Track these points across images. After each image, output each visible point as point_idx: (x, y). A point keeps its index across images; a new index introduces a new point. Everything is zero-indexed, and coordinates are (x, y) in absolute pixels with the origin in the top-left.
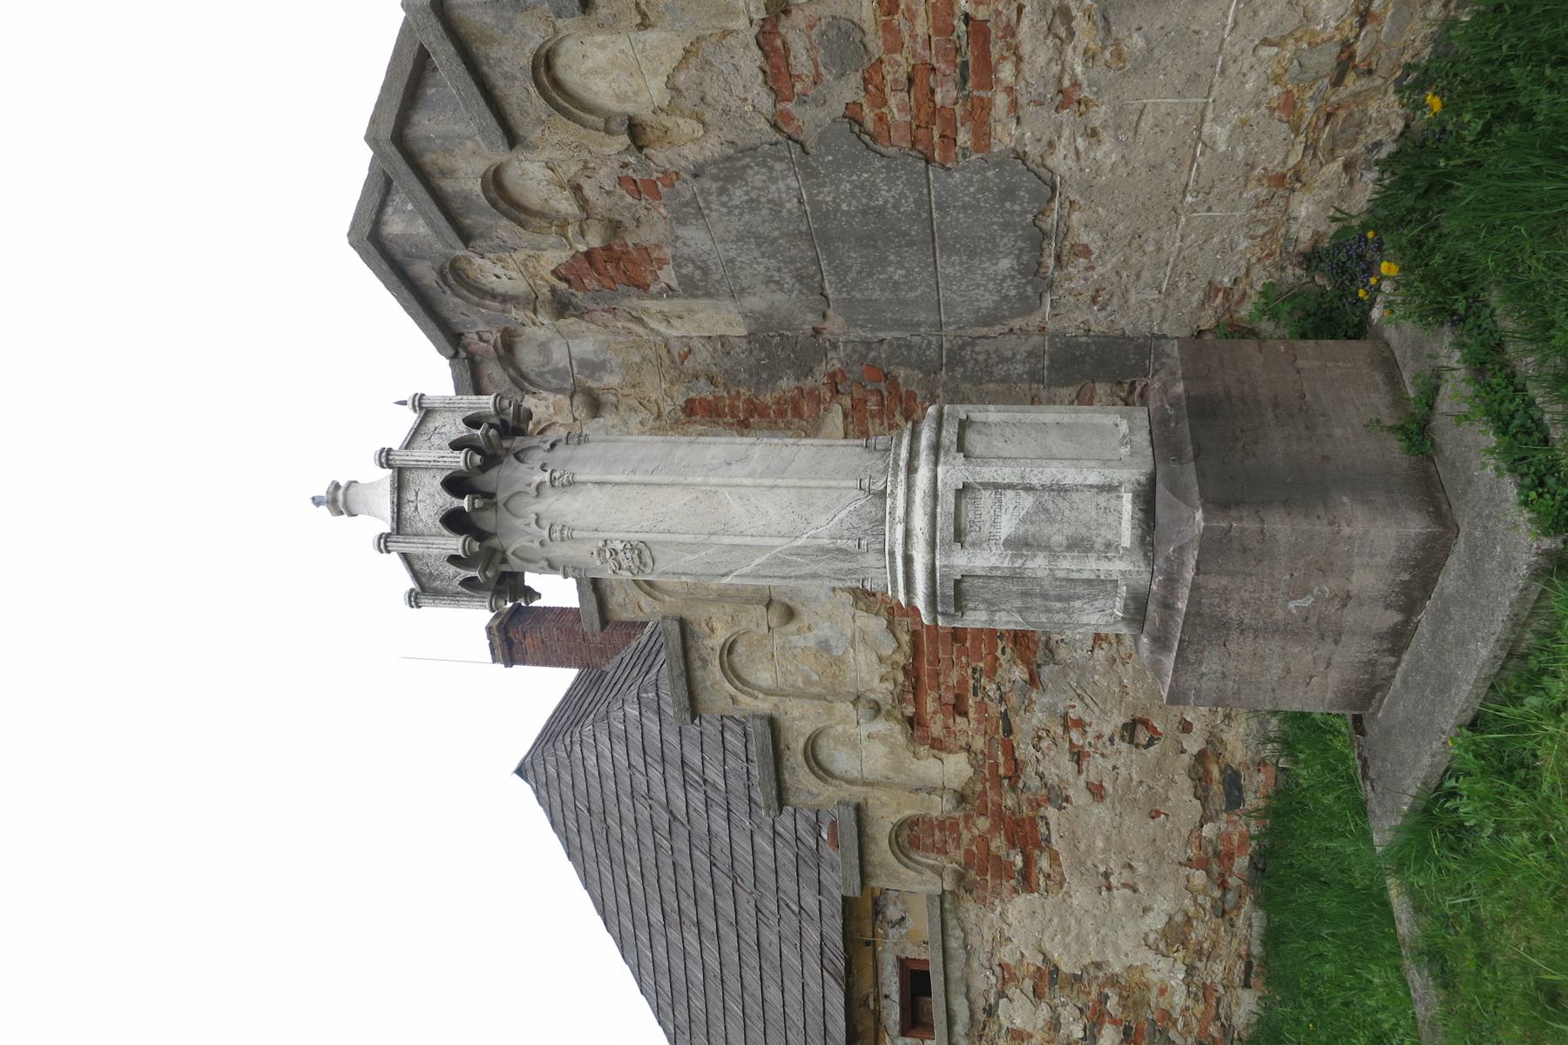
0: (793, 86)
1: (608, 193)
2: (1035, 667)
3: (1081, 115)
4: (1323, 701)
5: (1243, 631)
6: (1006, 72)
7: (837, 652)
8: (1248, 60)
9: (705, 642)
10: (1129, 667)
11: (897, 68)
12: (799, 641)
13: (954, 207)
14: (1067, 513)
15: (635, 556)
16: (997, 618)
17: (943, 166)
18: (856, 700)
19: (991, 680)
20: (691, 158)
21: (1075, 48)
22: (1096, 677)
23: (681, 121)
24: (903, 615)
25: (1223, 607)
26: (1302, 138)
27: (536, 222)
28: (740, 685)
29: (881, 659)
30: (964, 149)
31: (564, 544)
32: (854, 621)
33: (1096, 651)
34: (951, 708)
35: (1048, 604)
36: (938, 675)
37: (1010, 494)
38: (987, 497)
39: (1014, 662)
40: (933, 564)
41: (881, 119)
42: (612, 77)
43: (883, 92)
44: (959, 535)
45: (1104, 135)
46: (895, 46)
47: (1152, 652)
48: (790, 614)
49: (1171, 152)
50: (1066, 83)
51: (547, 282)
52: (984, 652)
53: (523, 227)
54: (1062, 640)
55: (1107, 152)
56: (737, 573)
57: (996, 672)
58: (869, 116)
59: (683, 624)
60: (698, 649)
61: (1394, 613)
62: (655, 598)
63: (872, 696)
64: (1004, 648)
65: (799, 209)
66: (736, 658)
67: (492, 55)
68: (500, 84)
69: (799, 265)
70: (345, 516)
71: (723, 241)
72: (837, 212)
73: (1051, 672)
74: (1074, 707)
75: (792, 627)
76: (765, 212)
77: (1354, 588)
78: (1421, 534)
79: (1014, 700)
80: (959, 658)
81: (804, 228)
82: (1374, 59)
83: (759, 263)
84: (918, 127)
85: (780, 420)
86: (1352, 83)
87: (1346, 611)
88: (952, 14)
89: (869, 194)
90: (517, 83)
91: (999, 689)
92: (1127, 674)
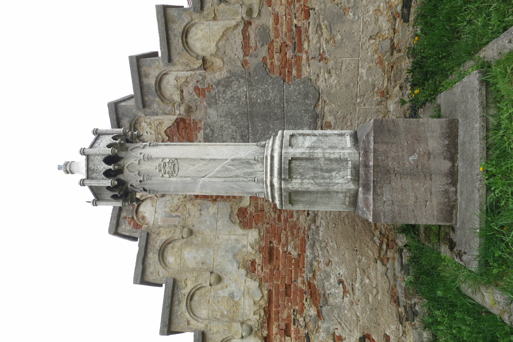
0: (249, 51)
1: (191, 94)
2: (320, 308)
3: (326, 64)
4: (434, 217)
5: (396, 174)
6: (306, 46)
7: (237, 299)
8: (367, 45)
9: (182, 291)
10: (359, 306)
11: (277, 45)
12: (221, 293)
13: (291, 101)
14: (328, 141)
15: (172, 166)
16: (304, 182)
17: (288, 83)
18: (242, 323)
19: (301, 316)
20: (217, 78)
21: (323, 38)
22: (346, 312)
23: (217, 60)
24: (266, 282)
25: (387, 162)
26: (386, 76)
27: (166, 101)
28: (192, 315)
29: (255, 303)
30: (294, 77)
31: (151, 148)
32: (245, 283)
33: (345, 298)
34: (283, 331)
35: (323, 174)
36: (279, 313)
37: (308, 137)
38: (300, 138)
39: (311, 306)
40: (281, 153)
41: (272, 63)
42: (202, 41)
43: (273, 53)
44: (290, 145)
45: (333, 72)
46: (277, 36)
47: (364, 194)
48: (219, 279)
49: (351, 79)
50: (321, 51)
51: (162, 137)
52: (298, 301)
53: (162, 102)
54: (330, 293)
55: (333, 80)
56: (208, 176)
57: (303, 312)
58: (269, 62)
59: (175, 281)
60: (178, 295)
61: (448, 162)
62: (166, 270)
63: (249, 323)
64: (306, 299)
65: (245, 101)
66: (193, 303)
67: (173, 27)
68: (172, 37)
69: (242, 129)
70: (70, 174)
71: (221, 116)
72: (256, 103)
73: (327, 310)
74: (337, 329)
75: (219, 286)
76: (235, 102)
77: (430, 148)
78: (446, 121)
79: (311, 326)
80: (287, 304)
81: (246, 110)
82: (400, 45)
83: (230, 128)
84: (282, 68)
85: (227, 199)
86: (396, 55)
87: (430, 162)
88: (292, 25)
89: (267, 95)
90: (177, 38)
91: (305, 320)
92: (358, 309)
